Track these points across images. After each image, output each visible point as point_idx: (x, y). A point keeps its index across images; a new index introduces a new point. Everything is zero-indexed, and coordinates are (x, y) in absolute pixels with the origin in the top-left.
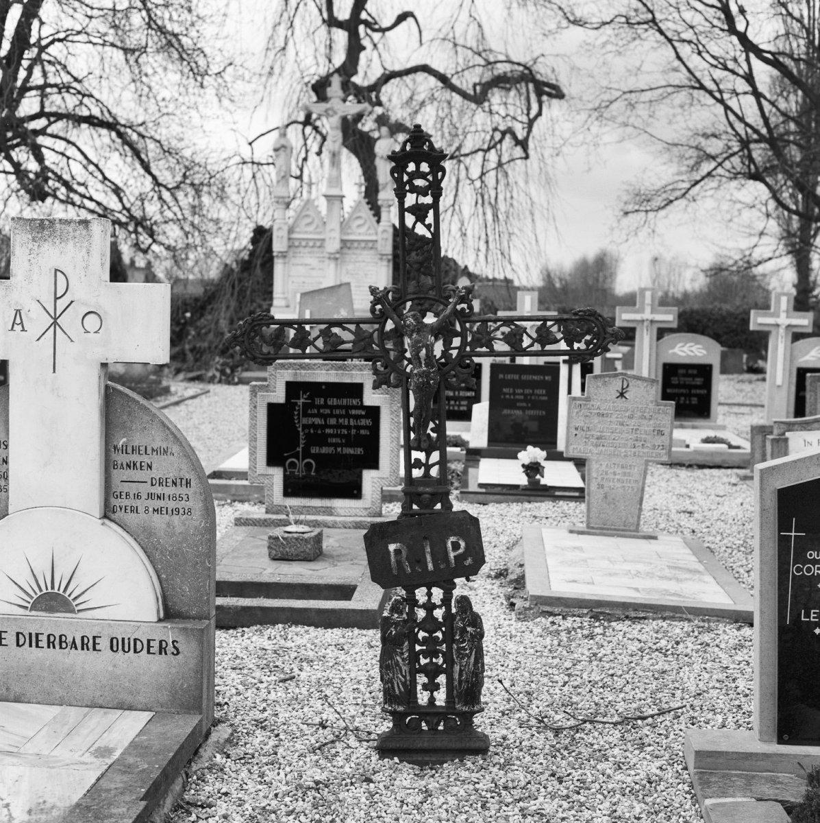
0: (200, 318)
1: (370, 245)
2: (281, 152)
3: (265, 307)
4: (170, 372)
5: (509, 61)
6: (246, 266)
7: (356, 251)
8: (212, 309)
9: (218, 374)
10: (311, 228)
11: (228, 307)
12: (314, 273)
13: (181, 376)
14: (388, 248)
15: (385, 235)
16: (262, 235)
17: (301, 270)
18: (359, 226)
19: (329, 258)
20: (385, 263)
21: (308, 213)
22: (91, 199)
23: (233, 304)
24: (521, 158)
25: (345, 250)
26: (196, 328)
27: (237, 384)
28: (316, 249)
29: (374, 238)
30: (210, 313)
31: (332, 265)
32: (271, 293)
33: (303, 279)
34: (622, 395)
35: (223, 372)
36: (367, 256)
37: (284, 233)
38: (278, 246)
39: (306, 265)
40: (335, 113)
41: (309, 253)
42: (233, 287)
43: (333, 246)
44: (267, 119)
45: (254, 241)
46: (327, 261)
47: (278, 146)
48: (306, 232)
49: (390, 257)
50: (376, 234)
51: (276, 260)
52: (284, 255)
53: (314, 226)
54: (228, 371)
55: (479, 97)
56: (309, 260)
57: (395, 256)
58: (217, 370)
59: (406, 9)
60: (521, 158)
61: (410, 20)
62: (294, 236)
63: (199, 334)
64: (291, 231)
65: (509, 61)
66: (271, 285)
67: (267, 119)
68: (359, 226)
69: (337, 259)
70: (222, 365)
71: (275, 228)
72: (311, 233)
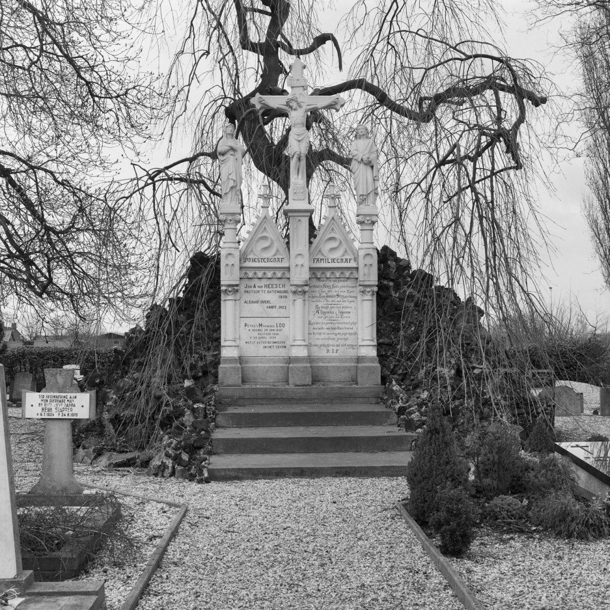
0: (122, 377)
4: (87, 455)
8: (140, 364)
9: (169, 463)
10: (269, 254)
11: (164, 361)
12: (274, 312)
13: (104, 461)
14: (373, 278)
15: (368, 261)
16: (203, 267)
17: (257, 309)
18: (332, 249)
19: (295, 292)
20: (368, 297)
21: (265, 234)
23: (171, 356)
24: (514, 168)
26: (118, 389)
27: (207, 481)
28: (275, 282)
29: (353, 264)
30: (138, 370)
31: (299, 301)
32: (218, 340)
33: (259, 321)
35: (177, 459)
36: (342, 288)
37: (235, 260)
38: (226, 278)
39: (263, 302)
41: (267, 286)
43: (300, 275)
44: (169, 153)
46: (291, 297)
48: (263, 260)
49: (376, 289)
50: (356, 259)
51: (223, 297)
52: (234, 289)
53: (273, 251)
54: (185, 457)
55: (424, 113)
56: (266, 296)
57: (381, 287)
58: (168, 455)
59: (325, 30)
60: (514, 168)
61: (329, 43)
62: (248, 264)
63: (122, 398)
64: (243, 257)
67: (169, 153)
69: (305, 292)
70: (176, 449)
71: (223, 253)
72: (269, 260)
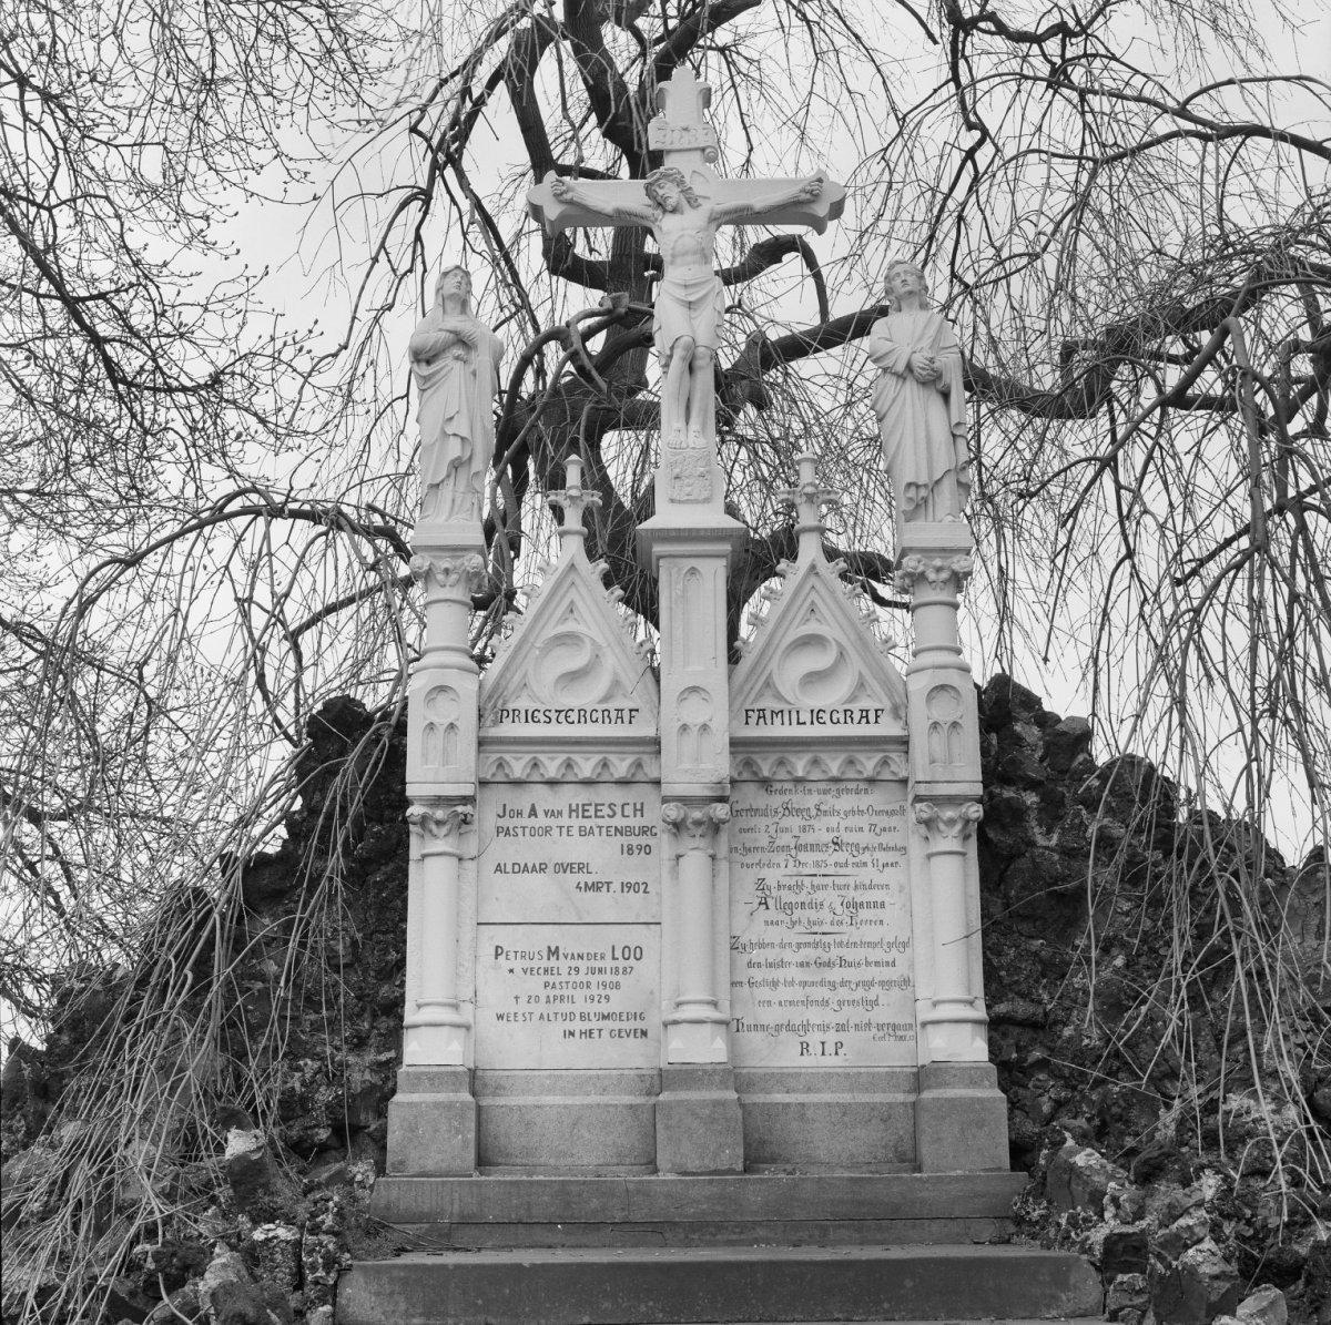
1: (869, 764)
2: (448, 364)
3: (360, 1077)
5: (975, 102)
6: (267, 883)
7: (800, 799)
18: (813, 678)
20: (948, 841)
21: (812, 628)
22: (1202, 562)
25: (751, 796)
31: (695, 861)
33: (550, 936)
34: (500, 1017)
36: (847, 815)
40: (693, 202)
42: (203, 968)
43: (695, 764)
45: (312, 770)
47: (435, 337)
52: (458, 812)
53: (600, 685)
65: (975, 102)
66: (396, 969)
68: (813, 678)
69: (715, 827)
